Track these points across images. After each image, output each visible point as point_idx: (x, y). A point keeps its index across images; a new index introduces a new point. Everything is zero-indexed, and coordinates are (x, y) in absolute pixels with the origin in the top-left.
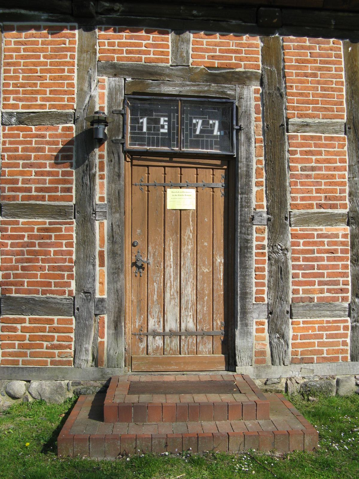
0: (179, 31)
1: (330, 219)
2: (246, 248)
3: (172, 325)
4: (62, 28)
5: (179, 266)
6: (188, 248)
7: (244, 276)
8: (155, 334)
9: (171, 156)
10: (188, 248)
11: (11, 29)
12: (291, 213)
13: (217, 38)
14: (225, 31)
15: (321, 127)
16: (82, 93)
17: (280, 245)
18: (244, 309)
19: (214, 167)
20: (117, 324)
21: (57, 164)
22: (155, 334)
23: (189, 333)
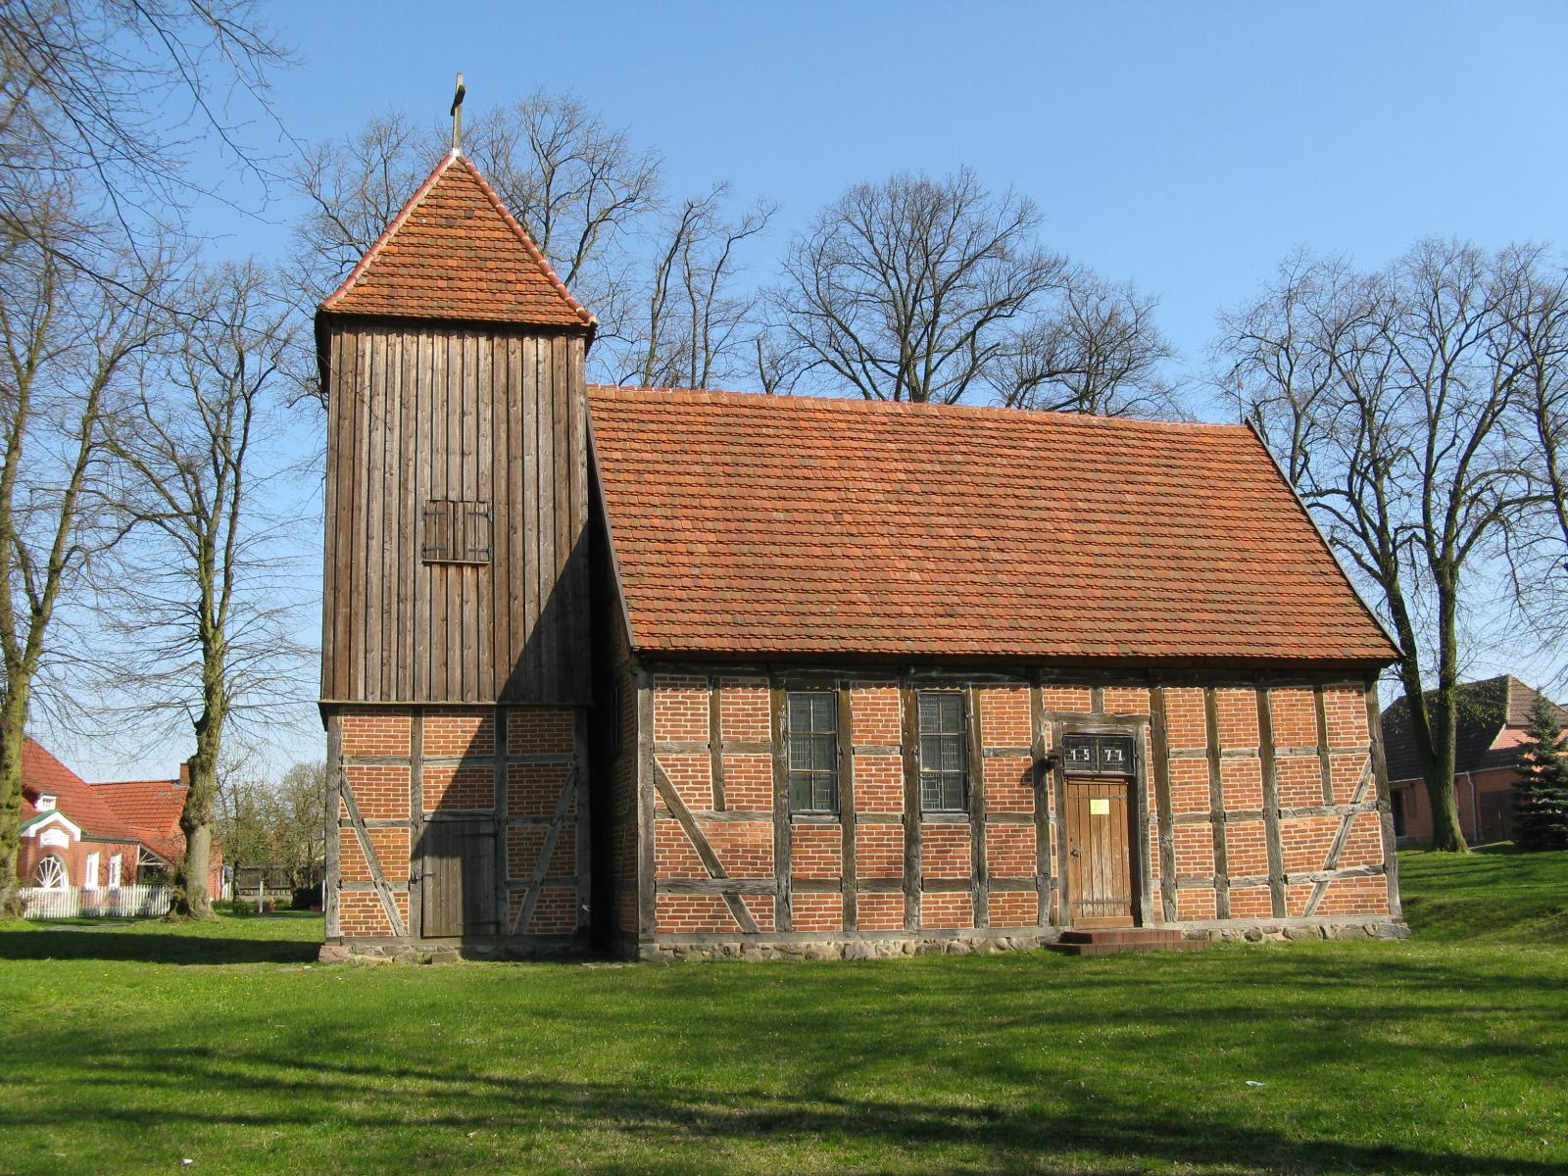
0: (1095, 687)
1: (1198, 819)
2: (1145, 840)
3: (1097, 896)
4: (1019, 687)
5: (1100, 854)
6: (1106, 841)
7: (1144, 860)
8: (1087, 902)
9: (1093, 777)
10: (1106, 841)
11: (985, 687)
12: (579, 343)
13: (1120, 691)
14: (1125, 685)
15: (1191, 754)
16: (1035, 734)
17: (1167, 838)
18: (257, 910)
19: (1120, 784)
20: (1065, 896)
21: (1022, 785)
22: (1087, 902)
23: (1109, 902)
